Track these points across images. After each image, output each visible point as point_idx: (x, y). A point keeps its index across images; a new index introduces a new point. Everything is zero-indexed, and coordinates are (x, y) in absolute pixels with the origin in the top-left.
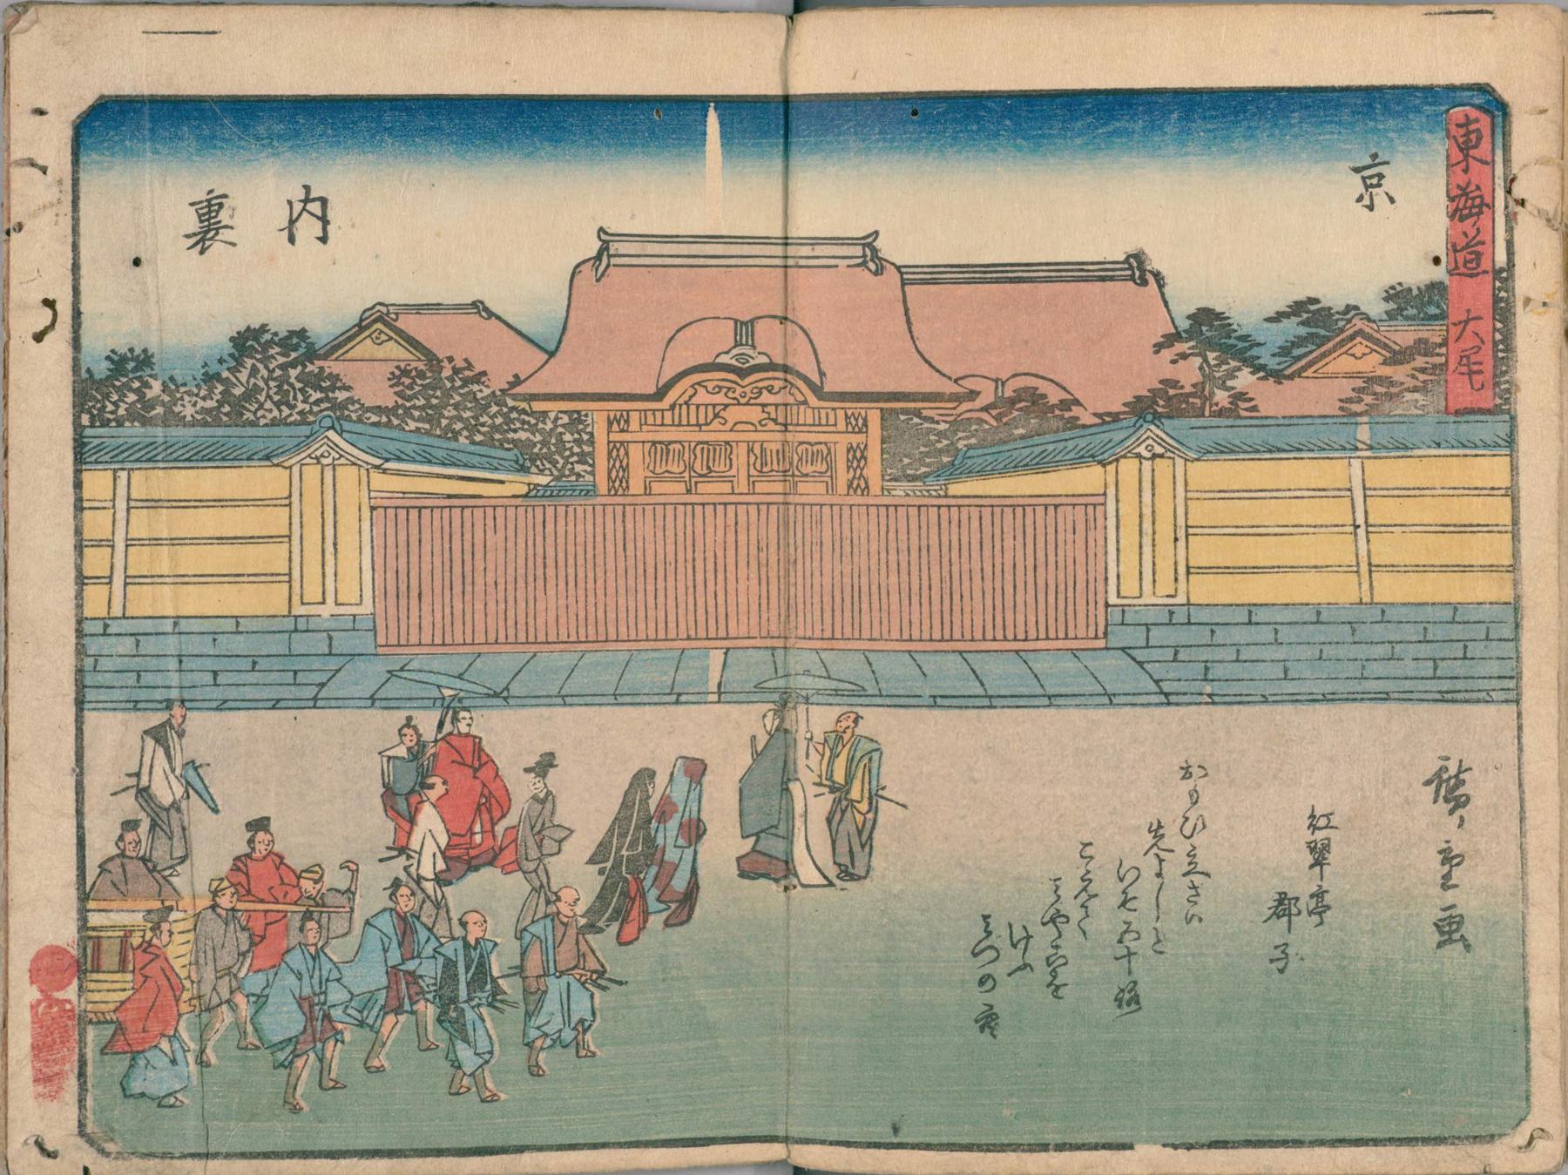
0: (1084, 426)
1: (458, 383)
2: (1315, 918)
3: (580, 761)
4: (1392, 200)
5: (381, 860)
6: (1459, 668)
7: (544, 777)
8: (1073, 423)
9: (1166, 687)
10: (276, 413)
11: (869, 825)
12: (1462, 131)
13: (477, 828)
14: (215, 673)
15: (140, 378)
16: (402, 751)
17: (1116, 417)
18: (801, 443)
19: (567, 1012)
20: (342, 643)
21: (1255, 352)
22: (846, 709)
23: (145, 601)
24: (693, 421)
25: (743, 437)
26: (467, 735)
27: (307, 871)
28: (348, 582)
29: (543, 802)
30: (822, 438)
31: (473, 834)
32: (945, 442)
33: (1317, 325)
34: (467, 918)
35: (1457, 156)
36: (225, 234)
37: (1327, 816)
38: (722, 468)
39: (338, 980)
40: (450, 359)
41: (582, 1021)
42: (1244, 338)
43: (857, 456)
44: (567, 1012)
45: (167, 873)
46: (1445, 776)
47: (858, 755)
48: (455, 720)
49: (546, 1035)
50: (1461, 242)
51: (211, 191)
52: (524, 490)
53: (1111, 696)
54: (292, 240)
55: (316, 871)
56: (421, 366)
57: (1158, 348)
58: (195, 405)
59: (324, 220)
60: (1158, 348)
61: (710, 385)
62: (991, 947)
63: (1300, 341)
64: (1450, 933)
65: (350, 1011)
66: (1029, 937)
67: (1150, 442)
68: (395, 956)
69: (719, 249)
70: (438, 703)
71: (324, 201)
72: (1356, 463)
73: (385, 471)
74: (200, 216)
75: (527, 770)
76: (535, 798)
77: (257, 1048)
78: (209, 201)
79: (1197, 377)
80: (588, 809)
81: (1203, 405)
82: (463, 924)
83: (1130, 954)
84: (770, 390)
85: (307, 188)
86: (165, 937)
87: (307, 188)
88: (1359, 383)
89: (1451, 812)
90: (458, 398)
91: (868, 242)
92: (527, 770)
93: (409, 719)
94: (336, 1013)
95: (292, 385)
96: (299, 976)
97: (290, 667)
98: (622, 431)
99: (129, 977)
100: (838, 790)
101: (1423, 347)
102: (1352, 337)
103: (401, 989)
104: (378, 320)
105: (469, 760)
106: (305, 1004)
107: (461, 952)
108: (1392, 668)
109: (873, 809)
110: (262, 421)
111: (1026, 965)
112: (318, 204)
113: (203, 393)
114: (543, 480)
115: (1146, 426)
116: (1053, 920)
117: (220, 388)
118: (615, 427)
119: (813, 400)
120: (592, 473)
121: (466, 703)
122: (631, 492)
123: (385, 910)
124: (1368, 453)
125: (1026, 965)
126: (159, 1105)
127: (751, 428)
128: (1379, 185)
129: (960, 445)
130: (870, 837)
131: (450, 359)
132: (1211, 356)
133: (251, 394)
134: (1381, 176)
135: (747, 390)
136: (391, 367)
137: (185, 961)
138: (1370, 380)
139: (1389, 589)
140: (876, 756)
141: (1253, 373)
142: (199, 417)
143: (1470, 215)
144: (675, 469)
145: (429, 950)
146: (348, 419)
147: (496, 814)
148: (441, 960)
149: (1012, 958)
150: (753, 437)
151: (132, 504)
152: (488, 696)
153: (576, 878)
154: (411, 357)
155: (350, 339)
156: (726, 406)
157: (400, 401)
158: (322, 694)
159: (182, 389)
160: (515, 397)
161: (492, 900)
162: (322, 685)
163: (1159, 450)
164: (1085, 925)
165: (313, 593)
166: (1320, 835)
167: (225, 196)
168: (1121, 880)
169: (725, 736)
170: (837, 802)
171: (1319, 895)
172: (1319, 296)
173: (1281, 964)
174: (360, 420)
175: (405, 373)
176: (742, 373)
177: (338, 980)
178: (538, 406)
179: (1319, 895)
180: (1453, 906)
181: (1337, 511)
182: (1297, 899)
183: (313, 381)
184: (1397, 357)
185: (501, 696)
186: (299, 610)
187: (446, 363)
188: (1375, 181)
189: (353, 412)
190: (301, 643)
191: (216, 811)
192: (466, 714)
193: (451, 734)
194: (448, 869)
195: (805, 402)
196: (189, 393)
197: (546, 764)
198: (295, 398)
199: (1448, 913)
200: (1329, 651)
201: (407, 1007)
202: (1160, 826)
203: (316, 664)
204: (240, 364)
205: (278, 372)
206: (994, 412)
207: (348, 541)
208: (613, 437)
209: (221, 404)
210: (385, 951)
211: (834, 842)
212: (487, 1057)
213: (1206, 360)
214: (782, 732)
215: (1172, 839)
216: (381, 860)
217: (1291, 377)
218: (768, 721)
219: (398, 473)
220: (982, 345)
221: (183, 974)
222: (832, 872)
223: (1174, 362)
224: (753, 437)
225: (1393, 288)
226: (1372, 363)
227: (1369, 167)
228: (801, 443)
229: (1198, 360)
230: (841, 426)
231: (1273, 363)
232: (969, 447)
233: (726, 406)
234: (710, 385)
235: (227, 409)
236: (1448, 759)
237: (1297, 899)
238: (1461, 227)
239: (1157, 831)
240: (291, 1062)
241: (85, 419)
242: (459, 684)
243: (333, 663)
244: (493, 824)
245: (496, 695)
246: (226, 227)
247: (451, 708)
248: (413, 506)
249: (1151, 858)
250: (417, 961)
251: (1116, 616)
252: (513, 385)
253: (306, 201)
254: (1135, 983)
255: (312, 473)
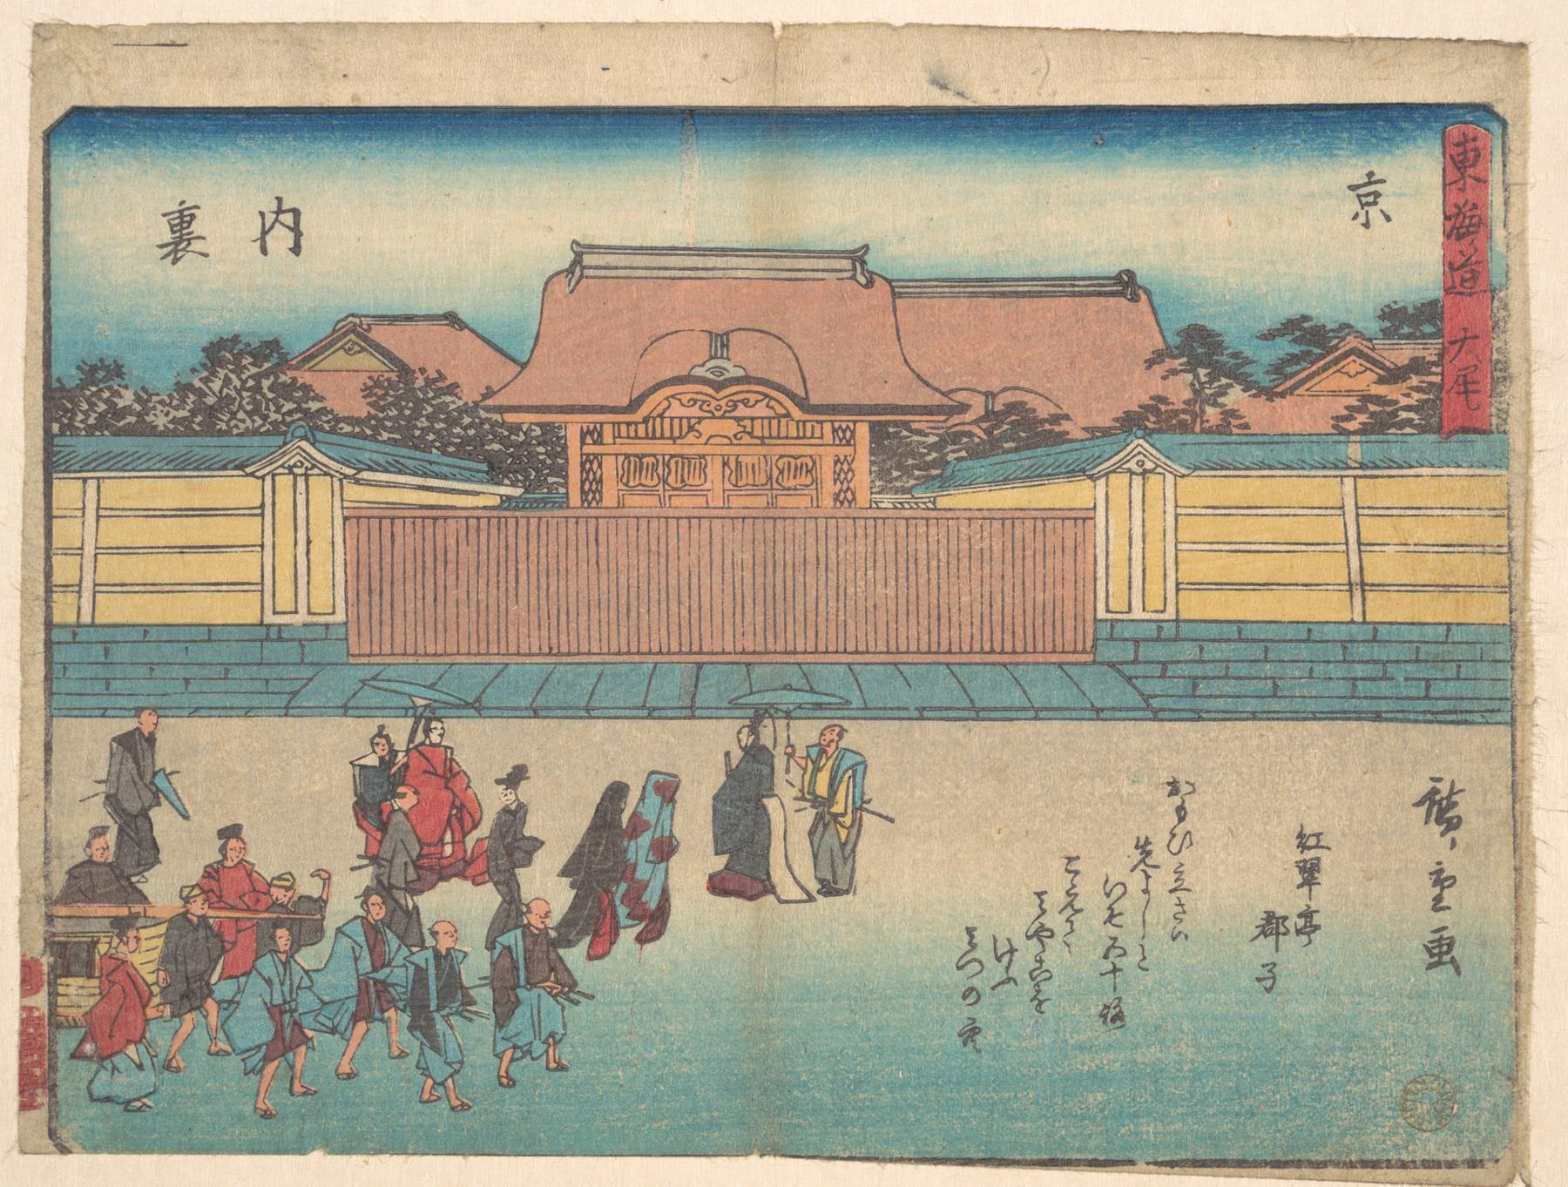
0: (1072, 441)
1: (431, 395)
2: (1304, 938)
3: (554, 769)
4: (1388, 219)
5: (353, 869)
6: (1451, 689)
7: (515, 789)
8: (1061, 438)
9: (1155, 703)
10: (248, 422)
11: (852, 839)
12: (1460, 150)
13: (448, 838)
14: (187, 680)
15: (110, 388)
16: (372, 760)
17: (1106, 432)
18: (781, 456)
19: (536, 1025)
20: (314, 652)
21: (1248, 369)
22: (826, 723)
23: (114, 610)
24: (667, 434)
25: (718, 450)
26: (439, 745)
27: (279, 878)
28: (322, 591)
29: (514, 813)
30: (809, 451)
31: (443, 845)
32: (934, 455)
33: (1310, 342)
34: (436, 928)
35: (1453, 175)
36: (196, 246)
37: (1318, 835)
38: (697, 482)
39: (309, 988)
40: (423, 370)
41: (552, 1035)
42: (1235, 355)
43: (843, 469)
44: (536, 1025)
45: (134, 879)
46: (1437, 798)
47: (843, 767)
48: (427, 731)
49: (515, 1047)
50: (1460, 260)
51: (183, 203)
52: (496, 501)
53: (1099, 710)
54: (264, 251)
55: (287, 880)
56: (393, 376)
57: (1150, 363)
58: (167, 414)
59: (296, 230)
60: (1150, 363)
61: (685, 399)
62: (975, 960)
63: (1293, 359)
64: (1440, 954)
65: (321, 1018)
66: (1012, 951)
67: (1141, 457)
68: (365, 964)
69: (699, 262)
70: (411, 712)
71: (296, 213)
72: (1349, 482)
73: (357, 482)
74: (172, 227)
75: (499, 782)
76: (506, 810)
77: (228, 1054)
78: (181, 212)
79: (1187, 394)
80: (559, 825)
81: (1194, 422)
82: (434, 934)
83: (1115, 970)
84: (745, 402)
85: (279, 200)
86: (132, 944)
87: (279, 200)
88: (1354, 402)
89: (1442, 834)
90: (430, 409)
91: (858, 256)
92: (499, 782)
93: (382, 728)
94: (307, 1021)
95: (264, 396)
96: (269, 982)
97: (266, 668)
98: (595, 443)
99: (95, 982)
100: (821, 804)
101: (1417, 366)
102: (1346, 355)
103: (371, 1000)
104: (354, 332)
105: (440, 772)
106: (276, 1012)
107: (432, 962)
108: (1385, 688)
109: (858, 824)
110: (235, 431)
111: (1009, 979)
112: (290, 215)
113: (175, 402)
114: (518, 492)
115: (1136, 442)
116: (1037, 934)
117: (192, 397)
118: (589, 440)
119: (797, 413)
120: (566, 485)
121: (439, 713)
122: (604, 504)
123: (356, 918)
124: (1360, 472)
125: (1009, 979)
126: (126, 1110)
127: (726, 441)
128: (1375, 203)
129: (951, 457)
130: (853, 851)
131: (423, 370)
132: (1202, 372)
133: (225, 401)
134: (1377, 195)
135: (723, 403)
136: (363, 379)
137: (153, 967)
138: (1366, 398)
139: (1382, 608)
140: (860, 769)
141: (1244, 390)
142: (171, 426)
143: (1469, 233)
144: (648, 482)
145: (399, 960)
146: (322, 429)
147: (468, 824)
148: (411, 969)
149: (996, 972)
150: (727, 450)
151: (102, 512)
152: (458, 707)
153: (547, 888)
154: (384, 368)
155: (325, 348)
156: (700, 419)
157: (373, 412)
158: (294, 704)
159: (155, 399)
160: (488, 409)
161: (460, 909)
162: (294, 694)
163: (1149, 465)
164: (1071, 939)
165: (285, 602)
166: (1309, 854)
167: (197, 207)
168: (1108, 895)
169: (701, 754)
170: (819, 818)
171: (1307, 915)
172: (1308, 312)
173: (1269, 983)
174: (333, 431)
175: (377, 384)
176: (719, 386)
177: (309, 988)
178: (511, 418)
179: (1307, 915)
180: (1444, 928)
181: (1331, 529)
182: (1285, 918)
183: (284, 391)
184: (1394, 375)
185: (476, 707)
186: (269, 618)
187: (418, 374)
188: (1371, 199)
189: (324, 422)
190: (274, 651)
191: (186, 817)
192: (439, 725)
193: (423, 743)
194: (419, 878)
195: (788, 415)
196: (161, 402)
197: (515, 777)
198: (267, 409)
199: (1437, 936)
200: (1319, 669)
201: (377, 1015)
202: (1147, 842)
203: (291, 672)
204: (214, 373)
205: (251, 383)
206: (984, 425)
207: (320, 547)
208: (586, 449)
209: (193, 413)
210: (356, 959)
211: (815, 857)
212: (456, 1066)
213: (1196, 376)
214: (756, 753)
215: (1159, 855)
216: (353, 869)
217: (1282, 395)
218: (743, 737)
219: (369, 483)
220: (975, 360)
221: (151, 979)
222: (813, 886)
223: (1164, 378)
224: (727, 450)
225: (1388, 306)
226: (1367, 382)
227: (1365, 185)
228: (781, 456)
229: (1190, 377)
230: (828, 438)
231: (1265, 381)
232: (959, 459)
233: (700, 419)
234: (685, 399)
235: (199, 419)
236: (1439, 780)
237: (1285, 918)
238: (1457, 246)
239: (1144, 848)
240: (262, 1069)
241: (56, 428)
242: (430, 694)
243: (306, 672)
244: (465, 834)
245: (467, 705)
246: (198, 238)
247: (425, 717)
248: (390, 515)
249: (1138, 875)
250: (387, 970)
251: (1104, 631)
252: (485, 397)
253: (279, 211)
254: (1120, 999)
255: (284, 481)
